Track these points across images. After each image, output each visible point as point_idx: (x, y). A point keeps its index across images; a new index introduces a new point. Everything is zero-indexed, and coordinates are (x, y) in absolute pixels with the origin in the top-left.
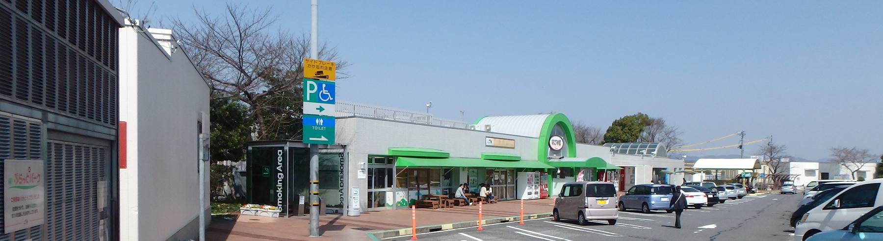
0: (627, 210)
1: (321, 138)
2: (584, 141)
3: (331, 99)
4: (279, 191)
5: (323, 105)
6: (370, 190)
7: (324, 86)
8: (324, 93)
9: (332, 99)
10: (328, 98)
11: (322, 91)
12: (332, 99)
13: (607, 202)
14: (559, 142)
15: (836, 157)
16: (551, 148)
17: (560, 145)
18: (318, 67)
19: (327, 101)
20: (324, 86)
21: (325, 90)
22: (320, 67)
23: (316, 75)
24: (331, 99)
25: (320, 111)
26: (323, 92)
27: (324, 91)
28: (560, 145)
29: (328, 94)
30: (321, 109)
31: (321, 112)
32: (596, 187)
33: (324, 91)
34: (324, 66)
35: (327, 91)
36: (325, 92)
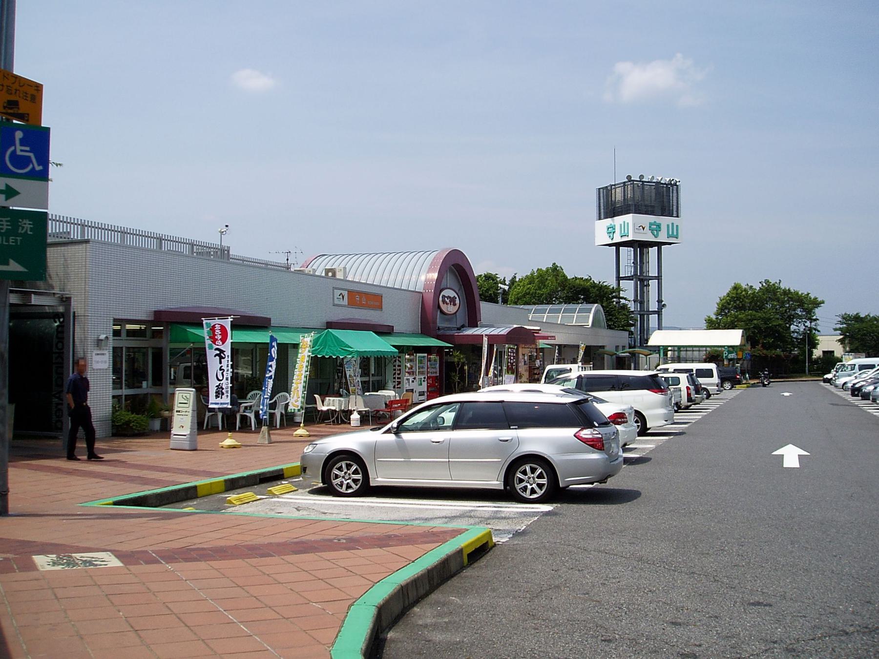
0: (511, 427)
1: (7, 264)
2: (492, 299)
3: (38, 168)
4: (258, 367)
5: (14, 183)
6: (118, 392)
7: (19, 135)
8: (19, 153)
9: (41, 168)
10: (31, 167)
11: (12, 148)
12: (41, 168)
13: (195, 503)
14: (453, 300)
15: (481, 526)
16: (442, 312)
17: (454, 305)
18: (9, 91)
19: (26, 173)
20: (19, 135)
21: (22, 144)
22: (14, 91)
23: (5, 107)
24: (38, 168)
25: (7, 199)
26: (14, 152)
27: (19, 148)
28: (454, 305)
29: (31, 155)
30: (10, 193)
31: (8, 201)
32: (253, 429)
33: (19, 148)
34: (21, 89)
35: (28, 149)
36: (20, 150)
